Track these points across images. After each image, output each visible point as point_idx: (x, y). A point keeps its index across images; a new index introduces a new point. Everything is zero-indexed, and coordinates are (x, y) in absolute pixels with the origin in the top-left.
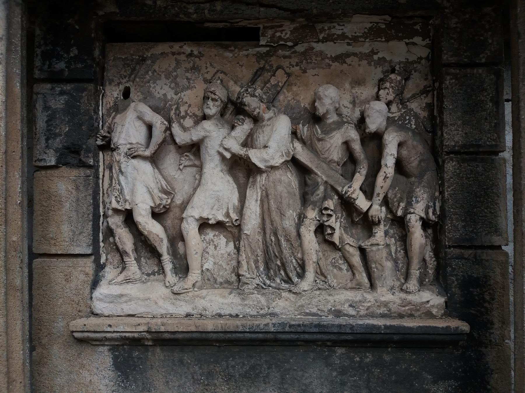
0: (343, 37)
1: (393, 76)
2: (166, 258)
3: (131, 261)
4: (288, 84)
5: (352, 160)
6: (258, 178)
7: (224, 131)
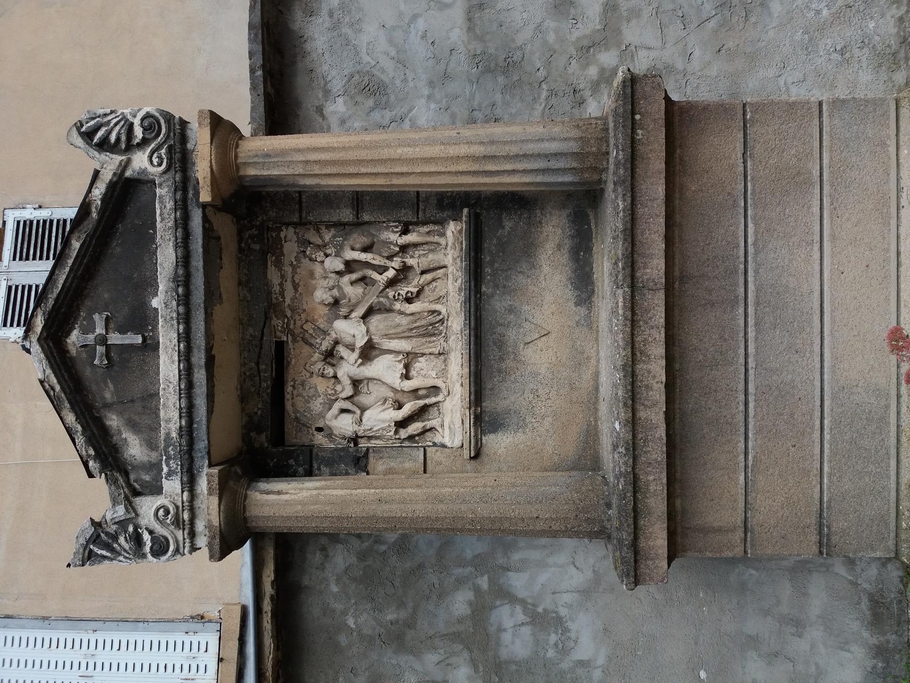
0: (281, 285)
1: (308, 253)
2: (427, 401)
3: (429, 424)
4: (313, 321)
5: (363, 279)
6: (375, 341)
7: (344, 363)
